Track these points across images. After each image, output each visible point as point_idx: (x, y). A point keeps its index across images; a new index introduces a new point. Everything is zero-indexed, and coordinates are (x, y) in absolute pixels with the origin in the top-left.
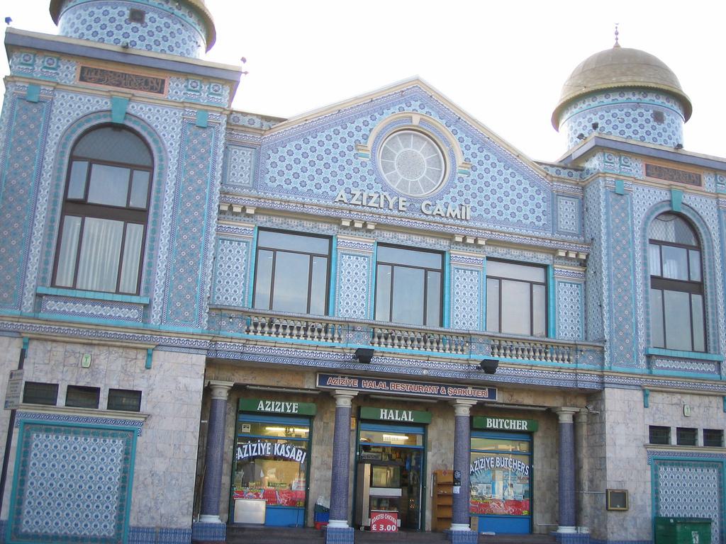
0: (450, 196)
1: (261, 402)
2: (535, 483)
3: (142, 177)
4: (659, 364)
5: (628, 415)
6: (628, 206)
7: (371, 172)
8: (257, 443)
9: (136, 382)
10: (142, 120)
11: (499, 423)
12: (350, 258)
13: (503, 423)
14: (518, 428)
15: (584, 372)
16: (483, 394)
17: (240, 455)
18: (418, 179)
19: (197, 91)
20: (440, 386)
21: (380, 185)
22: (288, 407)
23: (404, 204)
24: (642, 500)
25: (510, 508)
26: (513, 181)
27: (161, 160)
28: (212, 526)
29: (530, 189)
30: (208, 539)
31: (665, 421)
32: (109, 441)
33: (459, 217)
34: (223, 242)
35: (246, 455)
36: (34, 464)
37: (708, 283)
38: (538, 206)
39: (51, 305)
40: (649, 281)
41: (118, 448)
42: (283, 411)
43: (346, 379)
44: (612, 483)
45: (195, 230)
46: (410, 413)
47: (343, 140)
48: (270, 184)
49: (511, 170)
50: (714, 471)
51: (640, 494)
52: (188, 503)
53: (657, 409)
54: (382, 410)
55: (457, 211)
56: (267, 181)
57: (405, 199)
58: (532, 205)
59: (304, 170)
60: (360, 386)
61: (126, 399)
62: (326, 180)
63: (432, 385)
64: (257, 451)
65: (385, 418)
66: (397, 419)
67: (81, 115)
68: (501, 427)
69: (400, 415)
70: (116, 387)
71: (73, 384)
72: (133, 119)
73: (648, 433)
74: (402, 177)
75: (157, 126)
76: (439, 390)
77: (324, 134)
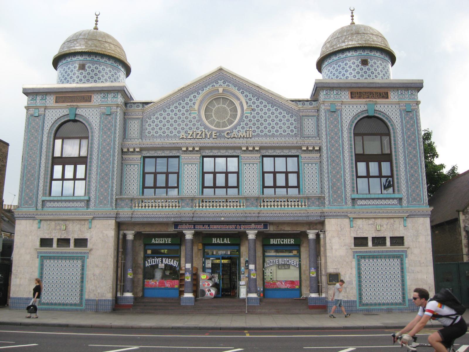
0: (241, 127)
1: (153, 239)
2: (302, 271)
3: (385, 140)
4: (359, 203)
5: (340, 232)
6: (338, 118)
7: (198, 121)
8: (155, 258)
9: (85, 235)
10: (382, 112)
11: (278, 241)
12: (188, 165)
13: (280, 241)
14: (288, 243)
15: (313, 211)
16: (261, 227)
17: (147, 265)
18: (225, 120)
19: (106, 98)
20: (237, 225)
21: (203, 127)
22: (166, 241)
23: (215, 134)
24: (350, 278)
25: (288, 285)
26: (277, 113)
27: (92, 133)
28: (127, 298)
29: (286, 116)
30: (125, 304)
31: (364, 234)
32: (75, 261)
33: (245, 136)
34: (246, 165)
35: (150, 264)
36: (45, 273)
37: (393, 154)
38: (292, 124)
39: (48, 204)
40: (354, 157)
41: (79, 264)
42: (164, 242)
43: (188, 225)
44: (331, 270)
45: (107, 163)
46: (228, 239)
47: (183, 107)
48: (148, 135)
49: (275, 107)
50: (398, 260)
51: (349, 274)
52: (110, 287)
53: (359, 228)
54: (213, 239)
55: (244, 134)
56: (147, 134)
57: (216, 132)
58: (288, 124)
59: (164, 125)
60: (194, 228)
61: (398, 241)
62: (175, 129)
63: (232, 224)
64: (155, 262)
65: (215, 242)
66: (221, 242)
67: (57, 118)
68: (279, 243)
69: (223, 241)
70: (77, 238)
71: (59, 237)
72: (79, 116)
73: (353, 241)
74: (217, 120)
75: (89, 118)
76: (236, 227)
77: (174, 106)
